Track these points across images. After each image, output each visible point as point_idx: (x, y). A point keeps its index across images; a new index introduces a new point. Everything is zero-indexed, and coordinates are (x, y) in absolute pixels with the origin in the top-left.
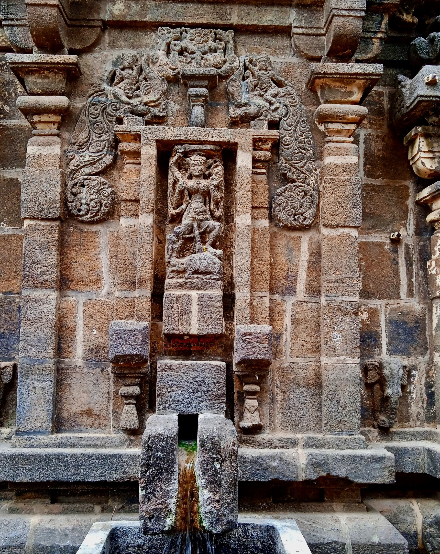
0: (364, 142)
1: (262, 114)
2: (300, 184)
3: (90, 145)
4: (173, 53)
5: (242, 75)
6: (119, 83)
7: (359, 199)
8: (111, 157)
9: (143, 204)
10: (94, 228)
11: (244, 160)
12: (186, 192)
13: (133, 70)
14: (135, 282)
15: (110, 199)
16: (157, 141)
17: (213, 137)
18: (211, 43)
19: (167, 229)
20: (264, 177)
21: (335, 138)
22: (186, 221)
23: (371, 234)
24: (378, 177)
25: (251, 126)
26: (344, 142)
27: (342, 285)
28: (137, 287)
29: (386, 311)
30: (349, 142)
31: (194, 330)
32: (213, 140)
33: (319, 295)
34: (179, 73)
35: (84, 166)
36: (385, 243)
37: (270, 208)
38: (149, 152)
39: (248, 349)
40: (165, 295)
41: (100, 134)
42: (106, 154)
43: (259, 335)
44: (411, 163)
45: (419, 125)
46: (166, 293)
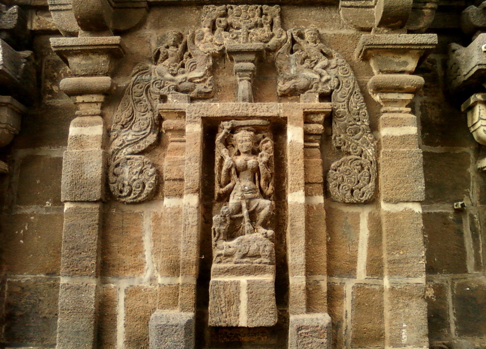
0: (420, 109)
1: (312, 86)
2: (357, 157)
3: (133, 124)
4: (218, 29)
5: (291, 48)
6: (164, 61)
7: (421, 172)
8: (155, 135)
9: (188, 183)
10: (138, 209)
11: (294, 135)
12: (233, 170)
13: (177, 47)
14: (179, 267)
15: (154, 179)
16: (202, 118)
17: (260, 112)
18: (257, 18)
19: (215, 209)
20: (317, 151)
21: (390, 108)
22: (233, 201)
23: (432, 204)
24: (436, 145)
25: (301, 99)
26: (401, 112)
27: (406, 266)
28: (181, 274)
29: (452, 287)
30: (406, 112)
31: (243, 322)
32: (262, 114)
33: (382, 276)
34: (224, 48)
35: (127, 145)
36: (448, 214)
37: (325, 184)
38: (194, 129)
39: (304, 345)
40: (211, 283)
41: (144, 112)
42: (150, 133)
43: (316, 329)
44: (472, 130)
45: (477, 92)
46: (213, 279)
